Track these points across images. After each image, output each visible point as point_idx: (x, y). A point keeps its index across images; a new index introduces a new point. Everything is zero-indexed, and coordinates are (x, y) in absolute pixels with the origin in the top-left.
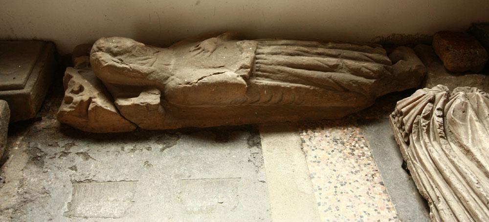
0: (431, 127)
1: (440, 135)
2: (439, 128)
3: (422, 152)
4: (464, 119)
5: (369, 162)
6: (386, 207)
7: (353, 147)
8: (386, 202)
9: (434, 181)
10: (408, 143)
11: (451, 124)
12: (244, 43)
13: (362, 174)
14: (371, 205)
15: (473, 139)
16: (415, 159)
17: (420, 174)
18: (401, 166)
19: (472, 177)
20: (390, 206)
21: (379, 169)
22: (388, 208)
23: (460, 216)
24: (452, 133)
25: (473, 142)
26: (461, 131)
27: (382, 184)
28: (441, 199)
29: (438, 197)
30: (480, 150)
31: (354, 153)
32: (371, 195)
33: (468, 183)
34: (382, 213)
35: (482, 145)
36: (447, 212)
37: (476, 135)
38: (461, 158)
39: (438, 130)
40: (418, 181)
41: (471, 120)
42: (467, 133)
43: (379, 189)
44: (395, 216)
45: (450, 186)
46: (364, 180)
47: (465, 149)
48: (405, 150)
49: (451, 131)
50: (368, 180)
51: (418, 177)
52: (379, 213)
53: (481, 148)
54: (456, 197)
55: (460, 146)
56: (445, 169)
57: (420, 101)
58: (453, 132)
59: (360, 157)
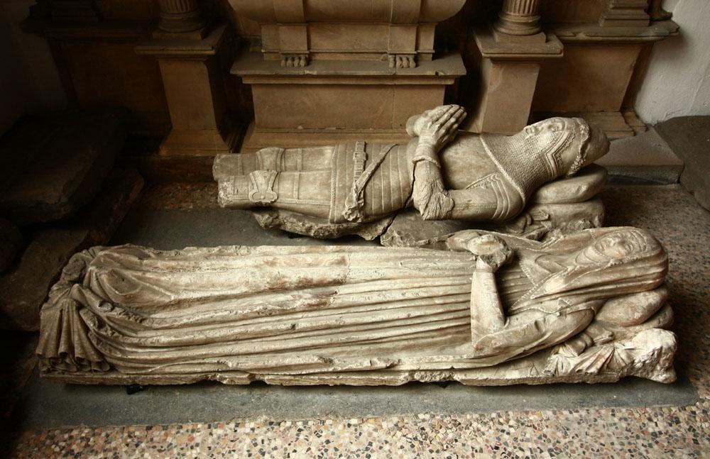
0: (116, 327)
1: (138, 321)
2: (129, 318)
3: (143, 354)
4: (134, 286)
5: (103, 435)
6: (190, 433)
7: (63, 452)
8: (182, 431)
9: (193, 358)
10: (113, 368)
11: (130, 303)
12: (488, 289)
13: (124, 450)
14: (182, 452)
15: (167, 289)
16: (144, 368)
17: (172, 371)
18: (128, 396)
19: (220, 314)
20: (190, 427)
21: (122, 424)
22: (193, 431)
23: (256, 348)
24: (141, 308)
25: (171, 292)
26: (148, 296)
27: (149, 428)
28: (223, 360)
29: (218, 362)
30: (186, 290)
31: (76, 452)
32: (165, 447)
33: (221, 322)
34: (198, 440)
35: (182, 286)
36: (243, 359)
37: (163, 284)
38: (180, 315)
39: (131, 320)
40: (176, 379)
41: (139, 278)
42: (155, 292)
43: (157, 434)
44: (207, 426)
45: (215, 342)
46: (134, 450)
47: (172, 305)
48: (120, 376)
49: (137, 308)
50: (137, 445)
51: (172, 376)
52: (197, 445)
53: (183, 288)
54: (231, 343)
55: (164, 309)
56: (192, 336)
57: (68, 321)
58: (141, 305)
59: (87, 446)
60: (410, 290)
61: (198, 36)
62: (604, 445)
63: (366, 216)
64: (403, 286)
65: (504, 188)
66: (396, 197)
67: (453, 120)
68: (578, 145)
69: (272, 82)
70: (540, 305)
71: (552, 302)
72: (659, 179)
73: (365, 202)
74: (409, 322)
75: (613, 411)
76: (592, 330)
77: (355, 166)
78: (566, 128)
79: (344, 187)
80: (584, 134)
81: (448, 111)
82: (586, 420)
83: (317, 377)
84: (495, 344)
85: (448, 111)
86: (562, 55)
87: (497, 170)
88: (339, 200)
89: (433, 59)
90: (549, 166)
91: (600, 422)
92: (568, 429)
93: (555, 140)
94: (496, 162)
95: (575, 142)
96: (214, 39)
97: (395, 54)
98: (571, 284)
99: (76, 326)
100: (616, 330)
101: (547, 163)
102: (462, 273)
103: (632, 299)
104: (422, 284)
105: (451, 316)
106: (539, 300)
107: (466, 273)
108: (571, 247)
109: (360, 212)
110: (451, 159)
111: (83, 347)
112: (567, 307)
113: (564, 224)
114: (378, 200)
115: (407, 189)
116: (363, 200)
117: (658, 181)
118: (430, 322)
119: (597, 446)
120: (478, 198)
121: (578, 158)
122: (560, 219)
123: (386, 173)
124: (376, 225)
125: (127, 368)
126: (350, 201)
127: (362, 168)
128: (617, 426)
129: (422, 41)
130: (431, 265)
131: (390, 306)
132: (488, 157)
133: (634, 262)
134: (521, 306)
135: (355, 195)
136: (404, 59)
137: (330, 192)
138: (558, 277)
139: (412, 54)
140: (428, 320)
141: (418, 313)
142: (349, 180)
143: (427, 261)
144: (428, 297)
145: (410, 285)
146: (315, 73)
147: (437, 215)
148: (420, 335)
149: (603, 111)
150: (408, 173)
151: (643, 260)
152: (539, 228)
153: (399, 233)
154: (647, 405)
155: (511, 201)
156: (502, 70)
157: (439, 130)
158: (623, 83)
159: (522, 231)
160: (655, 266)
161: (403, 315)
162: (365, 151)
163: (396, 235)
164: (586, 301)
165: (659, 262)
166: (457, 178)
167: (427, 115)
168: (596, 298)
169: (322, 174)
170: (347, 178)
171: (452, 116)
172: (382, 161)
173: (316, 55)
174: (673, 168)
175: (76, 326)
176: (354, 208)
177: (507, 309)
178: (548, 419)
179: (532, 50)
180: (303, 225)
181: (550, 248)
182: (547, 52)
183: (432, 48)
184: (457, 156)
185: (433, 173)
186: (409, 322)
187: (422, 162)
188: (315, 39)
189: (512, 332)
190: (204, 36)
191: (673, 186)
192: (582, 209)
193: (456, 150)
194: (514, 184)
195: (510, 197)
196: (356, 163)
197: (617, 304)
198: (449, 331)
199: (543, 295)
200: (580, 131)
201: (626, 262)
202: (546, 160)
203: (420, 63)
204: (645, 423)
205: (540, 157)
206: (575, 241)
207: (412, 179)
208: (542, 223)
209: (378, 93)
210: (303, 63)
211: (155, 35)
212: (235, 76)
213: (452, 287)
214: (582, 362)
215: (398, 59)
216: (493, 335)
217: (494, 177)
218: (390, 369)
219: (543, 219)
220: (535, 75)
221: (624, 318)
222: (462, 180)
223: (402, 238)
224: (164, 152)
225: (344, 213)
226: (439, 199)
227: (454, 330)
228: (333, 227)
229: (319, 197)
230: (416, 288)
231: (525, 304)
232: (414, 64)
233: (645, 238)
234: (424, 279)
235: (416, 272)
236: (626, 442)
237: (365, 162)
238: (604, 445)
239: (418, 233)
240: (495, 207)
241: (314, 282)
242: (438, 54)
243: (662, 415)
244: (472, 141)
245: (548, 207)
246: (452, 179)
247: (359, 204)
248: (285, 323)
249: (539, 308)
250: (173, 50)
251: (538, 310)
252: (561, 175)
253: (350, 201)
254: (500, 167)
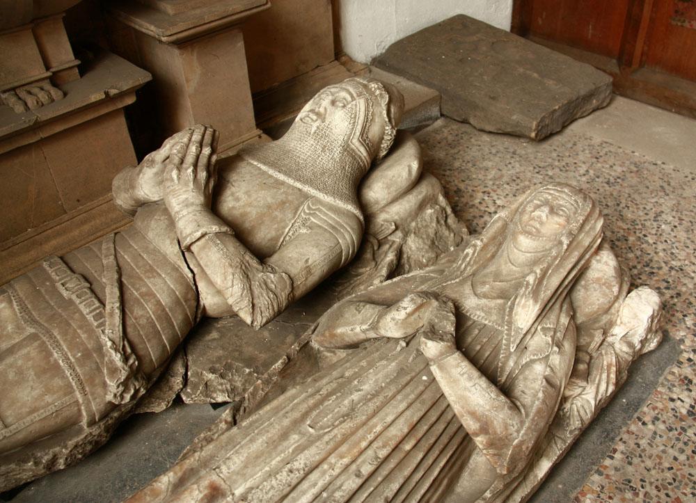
12: (470, 379)
60: (360, 460)
62: (672, 468)
63: (148, 378)
64: (346, 461)
65: (333, 216)
66: (180, 317)
68: (381, 113)
70: (528, 353)
71: (536, 338)
72: (425, 121)
73: (139, 358)
75: (639, 419)
77: (82, 307)
78: (355, 95)
79: (87, 355)
80: (381, 94)
81: (190, 140)
82: (631, 453)
84: (527, 448)
85: (190, 140)
87: (306, 197)
88: (93, 379)
89: (82, 74)
90: (360, 157)
91: (643, 442)
92: (630, 482)
93: (354, 118)
94: (298, 185)
95: (377, 110)
97: (14, 89)
98: (543, 300)
101: (356, 154)
102: (408, 378)
103: (592, 274)
104: (370, 437)
105: (436, 452)
106: (522, 348)
107: (413, 374)
108: (492, 249)
109: (137, 379)
110: (236, 213)
112: (555, 333)
113: (413, 224)
114: (154, 341)
115: (189, 296)
116: (133, 357)
117: (424, 123)
118: (417, 483)
119: (669, 475)
120: (315, 250)
122: (406, 220)
123: (144, 290)
124: (168, 381)
126: (113, 371)
127: (97, 304)
128: (658, 433)
129: (50, 50)
130: (355, 396)
132: (283, 183)
134: (508, 370)
135: (117, 358)
136: (35, 90)
137: (64, 377)
138: (523, 301)
139: (46, 78)
141: (395, 486)
142: (89, 337)
143: (344, 396)
144: (393, 450)
145: (356, 451)
147: (276, 309)
149: (318, 66)
150: (176, 269)
152: (391, 246)
153: (213, 371)
154: (654, 384)
155: (352, 229)
156: (195, 57)
157: (195, 177)
159: (374, 263)
160: (597, 219)
162: (73, 271)
163: (211, 376)
164: (561, 307)
166: (262, 236)
167: (153, 161)
169: (27, 357)
170: (84, 336)
171: (201, 145)
172: (120, 272)
174: (431, 101)
176: (127, 379)
178: (603, 487)
180: (36, 464)
181: (472, 266)
182: (250, 7)
183: (72, 56)
184: (241, 203)
185: (232, 249)
187: (203, 240)
189: (535, 415)
191: (440, 122)
192: (424, 194)
193: (233, 194)
195: (347, 223)
196: (78, 301)
197: (583, 290)
199: (522, 336)
200: (373, 93)
201: (577, 232)
202: (354, 151)
203: (66, 88)
204: (673, 407)
205: (345, 150)
206: (494, 238)
207: (190, 275)
208: (389, 238)
213: (411, 410)
215: (22, 94)
216: (520, 438)
217: (309, 208)
219: (390, 231)
220: (241, 44)
221: (606, 302)
222: (269, 236)
223: (222, 376)
225: (110, 397)
226: (266, 284)
228: (95, 431)
229: (48, 399)
230: (366, 448)
231: (511, 363)
232: (60, 93)
233: (566, 191)
234: (365, 428)
235: (348, 426)
236: (680, 445)
237: (92, 291)
238: (672, 468)
239: (241, 353)
240: (339, 251)
243: (674, 386)
244: (243, 170)
245: (388, 212)
246: (255, 242)
247: (131, 367)
249: (532, 357)
251: (533, 361)
252: (376, 162)
254: (307, 189)
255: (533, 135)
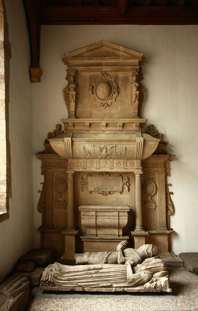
16: (61, 285)
26: (64, 270)
28: (77, 283)
61: (74, 230)
67: (125, 243)
69: (88, 240)
74: (115, 276)
76: (152, 278)
79: (103, 258)
83: (96, 288)
86: (148, 234)
87: (134, 254)
96: (78, 231)
99: (50, 274)
100: (157, 278)
111: (51, 279)
121: (151, 251)
125: (58, 285)
126: (104, 260)
129: (120, 232)
131: (111, 273)
133: (158, 263)
135: (105, 259)
140: (119, 276)
146: (97, 238)
148: (117, 279)
151: (159, 262)
158: (166, 243)
161: (114, 274)
165: (163, 263)
166: (126, 255)
168: (152, 272)
171: (124, 242)
173: (98, 217)
174: (181, 262)
175: (50, 274)
177: (134, 272)
179: (142, 233)
186: (115, 276)
188: (98, 232)
190: (75, 231)
191: (183, 268)
194: (138, 256)
198: (123, 279)
209: (111, 244)
210: (95, 236)
211: (66, 230)
212: (81, 238)
214: (151, 285)
218: (111, 286)
220: (144, 239)
224: (62, 258)
227: (124, 279)
241: (96, 268)
242: (123, 235)
248: (90, 276)
250: (69, 233)
253: (104, 260)
254: (135, 253)
255: (192, 271)
